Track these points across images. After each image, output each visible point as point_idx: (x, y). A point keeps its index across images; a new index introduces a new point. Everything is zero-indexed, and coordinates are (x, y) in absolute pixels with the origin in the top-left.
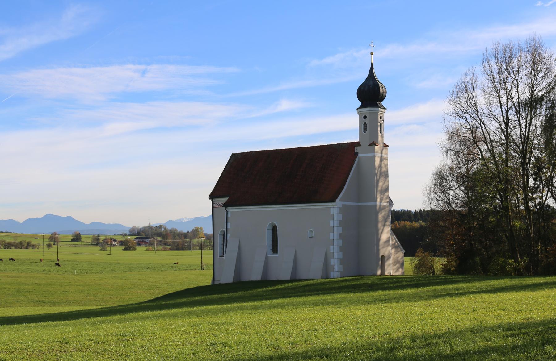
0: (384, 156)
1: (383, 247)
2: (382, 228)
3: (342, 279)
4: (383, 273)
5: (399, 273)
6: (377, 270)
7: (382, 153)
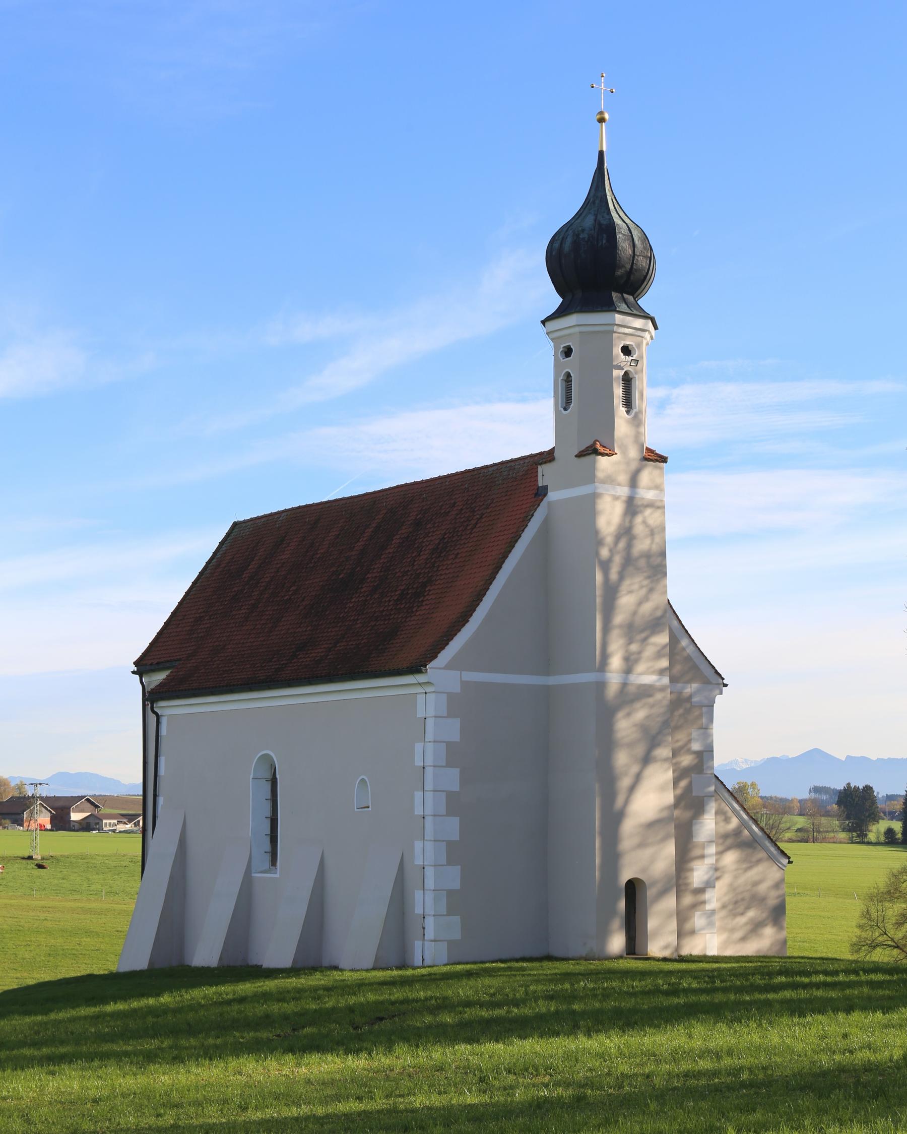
0: (646, 494)
1: (642, 845)
2: (635, 769)
3: (380, 975)
4: (633, 947)
5: (762, 944)
6: (604, 935)
7: (633, 482)
